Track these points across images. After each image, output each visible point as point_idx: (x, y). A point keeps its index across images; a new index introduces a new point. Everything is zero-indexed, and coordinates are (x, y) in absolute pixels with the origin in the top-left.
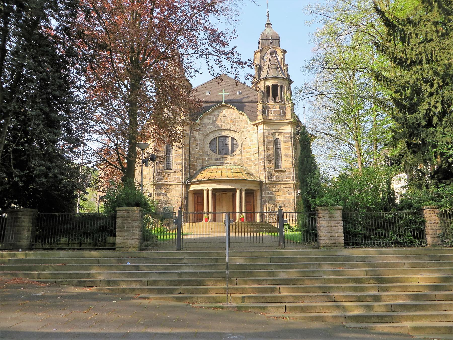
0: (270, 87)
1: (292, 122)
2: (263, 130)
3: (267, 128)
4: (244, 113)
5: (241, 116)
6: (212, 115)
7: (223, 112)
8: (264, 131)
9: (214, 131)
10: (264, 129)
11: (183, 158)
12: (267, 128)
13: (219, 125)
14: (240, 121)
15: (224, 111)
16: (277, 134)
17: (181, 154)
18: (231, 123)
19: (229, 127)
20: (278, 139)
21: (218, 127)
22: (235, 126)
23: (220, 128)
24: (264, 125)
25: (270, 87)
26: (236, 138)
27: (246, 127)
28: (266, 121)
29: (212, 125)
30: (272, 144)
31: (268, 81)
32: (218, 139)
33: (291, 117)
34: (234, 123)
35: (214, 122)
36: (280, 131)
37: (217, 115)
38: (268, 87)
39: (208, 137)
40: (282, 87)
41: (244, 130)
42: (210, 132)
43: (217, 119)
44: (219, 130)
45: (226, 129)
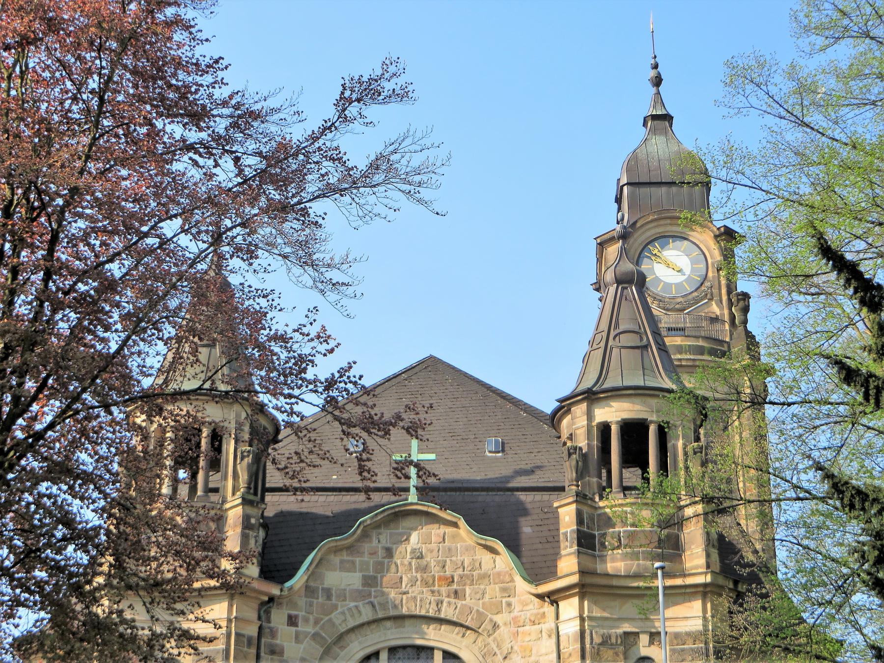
0: (614, 429)
7: (408, 539)
15: (414, 537)
18: (444, 590)
19: (434, 606)
21: (384, 606)
22: (460, 603)
23: (395, 607)
25: (614, 429)
27: (509, 605)
29: (360, 595)
31: (603, 403)
34: (455, 587)
37: (381, 553)
38: (605, 429)
39: (342, 648)
44: (389, 618)
45: (423, 613)
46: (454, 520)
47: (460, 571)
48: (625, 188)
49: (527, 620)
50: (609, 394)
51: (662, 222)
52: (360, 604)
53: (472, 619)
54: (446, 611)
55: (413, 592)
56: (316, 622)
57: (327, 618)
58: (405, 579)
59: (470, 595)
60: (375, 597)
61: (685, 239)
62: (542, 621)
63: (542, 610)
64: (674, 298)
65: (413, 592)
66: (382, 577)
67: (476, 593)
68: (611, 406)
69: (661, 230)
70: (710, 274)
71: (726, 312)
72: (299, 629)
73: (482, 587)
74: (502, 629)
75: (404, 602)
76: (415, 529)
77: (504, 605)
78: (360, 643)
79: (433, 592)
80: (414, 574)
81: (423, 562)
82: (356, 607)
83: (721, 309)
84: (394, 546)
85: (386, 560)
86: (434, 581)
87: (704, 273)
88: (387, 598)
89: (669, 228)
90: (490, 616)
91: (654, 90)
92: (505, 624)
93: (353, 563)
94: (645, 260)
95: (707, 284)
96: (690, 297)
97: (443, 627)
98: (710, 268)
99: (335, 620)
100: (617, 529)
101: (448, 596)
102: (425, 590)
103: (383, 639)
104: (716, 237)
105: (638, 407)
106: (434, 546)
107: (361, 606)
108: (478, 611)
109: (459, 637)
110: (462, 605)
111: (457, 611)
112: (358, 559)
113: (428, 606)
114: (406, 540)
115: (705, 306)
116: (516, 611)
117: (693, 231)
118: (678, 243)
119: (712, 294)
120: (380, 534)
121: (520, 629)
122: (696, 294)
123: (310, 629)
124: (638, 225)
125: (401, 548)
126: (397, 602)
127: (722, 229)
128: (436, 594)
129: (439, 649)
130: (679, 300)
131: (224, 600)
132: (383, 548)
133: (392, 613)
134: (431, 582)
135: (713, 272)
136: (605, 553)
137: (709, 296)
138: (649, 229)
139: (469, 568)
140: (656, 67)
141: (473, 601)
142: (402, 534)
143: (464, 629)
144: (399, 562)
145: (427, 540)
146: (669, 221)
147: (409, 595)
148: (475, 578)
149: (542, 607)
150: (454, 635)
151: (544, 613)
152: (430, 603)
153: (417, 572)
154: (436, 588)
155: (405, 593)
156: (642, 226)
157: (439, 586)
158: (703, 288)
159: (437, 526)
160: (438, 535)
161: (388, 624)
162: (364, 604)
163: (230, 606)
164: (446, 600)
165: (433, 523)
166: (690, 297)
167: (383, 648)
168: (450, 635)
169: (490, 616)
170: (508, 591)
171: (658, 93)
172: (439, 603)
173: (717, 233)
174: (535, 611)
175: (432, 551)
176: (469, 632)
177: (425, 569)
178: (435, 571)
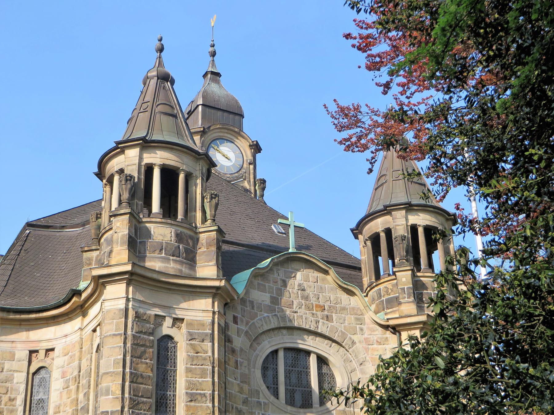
0: (420, 230)
1: (218, 288)
2: (124, 301)
3: (139, 297)
4: (356, 291)
5: (344, 296)
6: (269, 281)
7: (295, 276)
8: (127, 305)
9: (273, 329)
10: (128, 300)
11: (213, 406)
12: (139, 297)
13: (288, 312)
14: (344, 309)
15: (299, 275)
16: (168, 322)
17: (209, 392)
18: (319, 313)
19: (314, 323)
20: (169, 338)
21: (284, 317)
22: (330, 324)
23: (290, 321)
24: (128, 285)
25: (420, 230)
26: (331, 359)
27: (362, 330)
28: (139, 271)
29: (271, 310)
30: (152, 352)
31: (414, 213)
32: (281, 354)
33: (126, 256)
34: (326, 313)
35: (275, 301)
36: (179, 314)
37: (280, 282)
38: (414, 229)
39: (259, 344)
40: (188, 177)
41: (355, 338)
42: (264, 333)
43: (280, 293)
44: (284, 328)
45: (307, 327)
46: (327, 268)
47: (328, 303)
48: (200, 107)
49: (375, 341)
50: (420, 208)
51: (223, 130)
52: (270, 315)
53: (338, 336)
54: (321, 329)
55: (300, 312)
56: (247, 324)
57: (252, 322)
58: (295, 303)
59: (336, 319)
60: (278, 312)
61: (233, 143)
62: (386, 343)
63: (385, 336)
64: (225, 174)
65: (300, 312)
66: (281, 299)
67: (340, 319)
68: (419, 216)
69: (221, 134)
70: (245, 166)
71: (252, 188)
72: (239, 326)
73: (343, 315)
74: (358, 344)
75: (295, 318)
76: (298, 270)
77: (358, 329)
78: (269, 342)
79: (313, 314)
80: (300, 300)
81: (306, 293)
82: (268, 317)
83: (250, 186)
84: (287, 280)
85: (283, 288)
86: (313, 307)
87: (242, 164)
88: (285, 314)
89: (226, 135)
90: (349, 335)
91: (211, 58)
92: (360, 342)
93: (265, 286)
94: (212, 149)
95: (243, 170)
96: (234, 175)
97: (318, 339)
98: (245, 162)
99: (256, 324)
100: (429, 291)
101: (323, 319)
102: (307, 312)
103: (282, 341)
104: (250, 146)
105: (434, 220)
106: (311, 284)
107: (271, 317)
108: (341, 331)
109: (328, 347)
110: (331, 326)
111: (328, 329)
112: (267, 284)
113: (310, 323)
114: (293, 277)
115: (240, 183)
116: (366, 334)
117: (238, 139)
118: (229, 144)
119: (245, 177)
120: (279, 270)
121: (369, 346)
122: (236, 174)
123: (243, 328)
124: (211, 128)
125: (291, 281)
126: (291, 318)
127: (255, 142)
128: (315, 316)
129: (314, 353)
130: (229, 176)
131: (208, 297)
132: (281, 279)
133: (288, 324)
134: (311, 307)
135: (247, 165)
136: (423, 305)
137: (244, 177)
138: (216, 132)
139: (334, 302)
140: (213, 46)
141: (338, 324)
142: (292, 273)
143: (331, 342)
144: (290, 290)
145: (307, 280)
146: (226, 131)
147: (298, 314)
148: (338, 309)
149: (385, 334)
150: (324, 345)
151: (387, 338)
152: (311, 322)
153: (302, 299)
154: (314, 312)
155: (296, 312)
156: (213, 130)
157: (316, 311)
158: (241, 172)
159: (312, 271)
160: (314, 277)
161: (285, 332)
162: (272, 316)
163: (213, 303)
164: (321, 321)
165: (310, 268)
166: (234, 175)
167: (281, 348)
168: (322, 345)
169: (349, 335)
170: (360, 321)
171: (213, 61)
172: (317, 322)
173: (251, 144)
174: (380, 336)
175: (310, 287)
176: (334, 344)
177: (306, 298)
178: (313, 300)
